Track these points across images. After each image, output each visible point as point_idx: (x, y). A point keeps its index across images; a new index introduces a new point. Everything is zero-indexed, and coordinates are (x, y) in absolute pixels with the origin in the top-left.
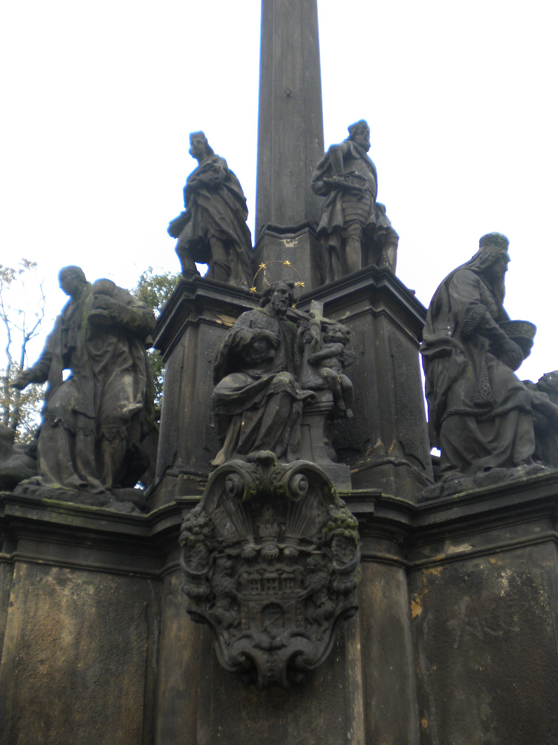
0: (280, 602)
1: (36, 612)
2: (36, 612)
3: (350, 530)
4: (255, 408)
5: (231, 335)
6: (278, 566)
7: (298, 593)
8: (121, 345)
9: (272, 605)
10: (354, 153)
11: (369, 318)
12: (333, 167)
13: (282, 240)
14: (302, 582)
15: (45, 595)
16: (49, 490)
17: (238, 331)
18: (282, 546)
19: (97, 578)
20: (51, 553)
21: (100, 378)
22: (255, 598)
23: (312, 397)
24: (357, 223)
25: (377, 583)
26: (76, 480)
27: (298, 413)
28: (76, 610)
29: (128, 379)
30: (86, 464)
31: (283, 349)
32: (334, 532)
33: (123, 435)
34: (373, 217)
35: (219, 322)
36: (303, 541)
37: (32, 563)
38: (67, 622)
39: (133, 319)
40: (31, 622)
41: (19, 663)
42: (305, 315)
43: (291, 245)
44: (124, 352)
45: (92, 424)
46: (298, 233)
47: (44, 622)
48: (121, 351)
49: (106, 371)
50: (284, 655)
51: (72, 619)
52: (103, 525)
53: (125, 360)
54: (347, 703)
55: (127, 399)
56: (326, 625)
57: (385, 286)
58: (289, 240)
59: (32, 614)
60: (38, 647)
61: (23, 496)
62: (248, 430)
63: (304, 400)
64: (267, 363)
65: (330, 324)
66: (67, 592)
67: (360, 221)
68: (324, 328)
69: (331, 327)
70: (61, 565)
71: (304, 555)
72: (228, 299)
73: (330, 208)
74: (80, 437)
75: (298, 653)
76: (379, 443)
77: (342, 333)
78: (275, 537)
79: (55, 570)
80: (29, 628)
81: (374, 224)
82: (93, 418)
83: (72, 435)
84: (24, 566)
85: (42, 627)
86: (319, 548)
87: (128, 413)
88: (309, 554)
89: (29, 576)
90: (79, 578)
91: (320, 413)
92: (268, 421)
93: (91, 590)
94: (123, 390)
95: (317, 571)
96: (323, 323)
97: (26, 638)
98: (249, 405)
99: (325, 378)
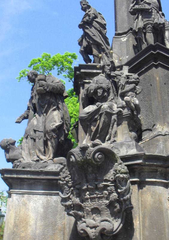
0: (98, 207)
1: (20, 212)
2: (20, 212)
3: (123, 174)
5: (86, 90)
7: (105, 202)
8: (51, 100)
13: (121, 39)
15: (23, 205)
16: (24, 164)
17: (89, 87)
18: (96, 183)
23: (120, 111)
24: (149, 24)
25: (148, 193)
27: (115, 119)
31: (111, 91)
32: (116, 176)
33: (54, 137)
38: (32, 215)
40: (18, 216)
41: (14, 233)
44: (53, 102)
45: (42, 134)
46: (127, 34)
47: (23, 216)
48: (52, 102)
50: (98, 229)
51: (33, 214)
55: (55, 121)
57: (152, 52)
58: (123, 38)
59: (18, 213)
60: (21, 226)
61: (13, 169)
63: (117, 113)
64: (104, 99)
65: (131, 75)
67: (150, 23)
68: (128, 77)
69: (130, 77)
73: (137, 20)
77: (135, 79)
78: (93, 180)
80: (17, 219)
81: (157, 23)
82: (42, 132)
85: (22, 218)
87: (25, 187)
88: (108, 186)
92: (101, 126)
93: (41, 202)
95: (112, 193)
97: (16, 223)
99: (126, 102)
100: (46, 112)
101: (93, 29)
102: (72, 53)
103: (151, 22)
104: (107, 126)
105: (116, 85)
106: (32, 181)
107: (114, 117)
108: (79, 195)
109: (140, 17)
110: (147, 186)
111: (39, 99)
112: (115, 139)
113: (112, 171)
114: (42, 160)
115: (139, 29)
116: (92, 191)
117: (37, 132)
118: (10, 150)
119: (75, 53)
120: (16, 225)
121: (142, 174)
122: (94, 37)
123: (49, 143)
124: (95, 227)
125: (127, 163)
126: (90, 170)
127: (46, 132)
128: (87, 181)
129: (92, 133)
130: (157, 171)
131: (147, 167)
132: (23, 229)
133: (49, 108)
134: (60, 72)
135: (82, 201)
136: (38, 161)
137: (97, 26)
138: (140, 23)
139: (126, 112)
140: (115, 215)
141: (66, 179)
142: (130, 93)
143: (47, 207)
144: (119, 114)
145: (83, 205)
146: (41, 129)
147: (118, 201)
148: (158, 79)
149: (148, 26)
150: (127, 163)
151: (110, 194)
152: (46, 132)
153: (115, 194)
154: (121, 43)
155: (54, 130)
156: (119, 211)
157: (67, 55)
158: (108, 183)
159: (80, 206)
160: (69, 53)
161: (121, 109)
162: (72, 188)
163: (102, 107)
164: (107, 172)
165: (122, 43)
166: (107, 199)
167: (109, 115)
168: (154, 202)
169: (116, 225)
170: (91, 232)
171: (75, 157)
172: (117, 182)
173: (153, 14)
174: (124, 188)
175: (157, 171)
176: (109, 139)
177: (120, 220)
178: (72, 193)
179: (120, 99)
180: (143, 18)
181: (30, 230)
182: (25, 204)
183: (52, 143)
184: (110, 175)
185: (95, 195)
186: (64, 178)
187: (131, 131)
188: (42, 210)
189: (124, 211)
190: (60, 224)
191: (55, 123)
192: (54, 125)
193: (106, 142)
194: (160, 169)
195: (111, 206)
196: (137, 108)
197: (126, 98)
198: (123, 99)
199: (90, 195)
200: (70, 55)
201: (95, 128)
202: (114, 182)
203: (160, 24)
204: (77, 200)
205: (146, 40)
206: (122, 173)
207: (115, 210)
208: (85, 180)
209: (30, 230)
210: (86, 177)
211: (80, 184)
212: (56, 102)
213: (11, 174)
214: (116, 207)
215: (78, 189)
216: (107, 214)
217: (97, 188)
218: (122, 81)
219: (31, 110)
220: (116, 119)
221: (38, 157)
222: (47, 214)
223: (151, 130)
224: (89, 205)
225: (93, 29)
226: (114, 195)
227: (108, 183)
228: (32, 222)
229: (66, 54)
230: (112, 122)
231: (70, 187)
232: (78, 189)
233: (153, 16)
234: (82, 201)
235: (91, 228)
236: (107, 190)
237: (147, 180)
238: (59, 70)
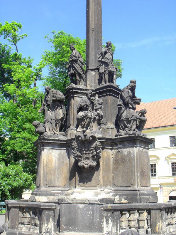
9: (88, 157)
10: (108, 52)
12: (93, 135)
23: (95, 117)
29: (61, 110)
30: (54, 129)
31: (90, 106)
42: (94, 98)
43: (93, 74)
50: (89, 165)
55: (61, 115)
64: (86, 109)
68: (98, 100)
69: (99, 101)
72: (80, 91)
74: (53, 124)
75: (91, 165)
81: (111, 71)
87: (50, 146)
88: (93, 149)
93: (57, 153)
94: (60, 113)
96: (98, 100)
99: (98, 113)
100: (56, 110)
101: (77, 65)
102: (18, 24)
103: (108, 69)
104: (89, 123)
105: (93, 104)
106: (54, 143)
107: (92, 119)
108: (80, 152)
109: (103, 65)
110: (105, 149)
111: (52, 102)
112: (92, 129)
113: (94, 144)
114: (56, 133)
115: (102, 72)
116: (86, 151)
117: (52, 120)
118: (38, 127)
119: (21, 24)
120: (47, 163)
121: (103, 145)
122: (78, 70)
123: (58, 125)
124: (87, 164)
125: (100, 140)
126: (86, 143)
127: (56, 120)
128: (85, 147)
129: (82, 125)
130: (109, 144)
131: (106, 142)
132: (50, 164)
133: (57, 108)
134: (6, 37)
135: (82, 154)
136: (54, 134)
137: (80, 64)
138: (103, 69)
139: (97, 118)
140: (94, 160)
141: (76, 145)
142: (99, 109)
143: (60, 155)
144: (95, 118)
145: (82, 156)
146: (54, 118)
147: (96, 155)
148: (110, 101)
149: (107, 71)
150: (100, 140)
151: (93, 152)
152: (56, 120)
153: (95, 152)
154: (91, 76)
155: (60, 120)
156: (96, 159)
157: (14, 24)
158: (93, 148)
159: (81, 156)
160: (16, 23)
161: (95, 116)
162: (78, 149)
163: (88, 115)
164: (93, 144)
165: (92, 76)
166: (92, 154)
167: (91, 118)
168: (107, 156)
169: (94, 164)
170: (86, 166)
171: (81, 138)
172: (96, 148)
173: (110, 65)
174: (99, 151)
175: (109, 144)
176: (90, 128)
177: (96, 162)
178: (78, 151)
179: (95, 112)
180: (105, 66)
181: (53, 165)
182: (51, 154)
183: (59, 125)
184: (94, 145)
185: (87, 153)
186: (75, 145)
187: (98, 125)
188: (58, 156)
189: (97, 158)
190: (65, 162)
193: (88, 129)
194: (110, 143)
195: (93, 157)
196: (102, 116)
197: (98, 111)
198: (96, 111)
199: (85, 152)
200: (16, 25)
201: (84, 123)
202: (95, 148)
203: (112, 71)
204: (80, 154)
205: (105, 78)
207: (95, 158)
208: (83, 146)
209: (53, 165)
211: (81, 148)
212: (61, 105)
213: (45, 140)
214: (95, 157)
215: (80, 150)
216: (91, 160)
217: (88, 150)
218: (96, 103)
219: (46, 106)
220: (93, 120)
221: (54, 132)
222: (60, 158)
223: (105, 124)
224: (84, 156)
225: (77, 65)
226: (95, 153)
227: (93, 148)
228: (54, 161)
229: (12, 23)
230: (91, 121)
231: (77, 149)
232: (80, 150)
233: (109, 66)
234: (82, 154)
235: (86, 164)
236: (92, 151)
237: (105, 147)
238: (6, 35)
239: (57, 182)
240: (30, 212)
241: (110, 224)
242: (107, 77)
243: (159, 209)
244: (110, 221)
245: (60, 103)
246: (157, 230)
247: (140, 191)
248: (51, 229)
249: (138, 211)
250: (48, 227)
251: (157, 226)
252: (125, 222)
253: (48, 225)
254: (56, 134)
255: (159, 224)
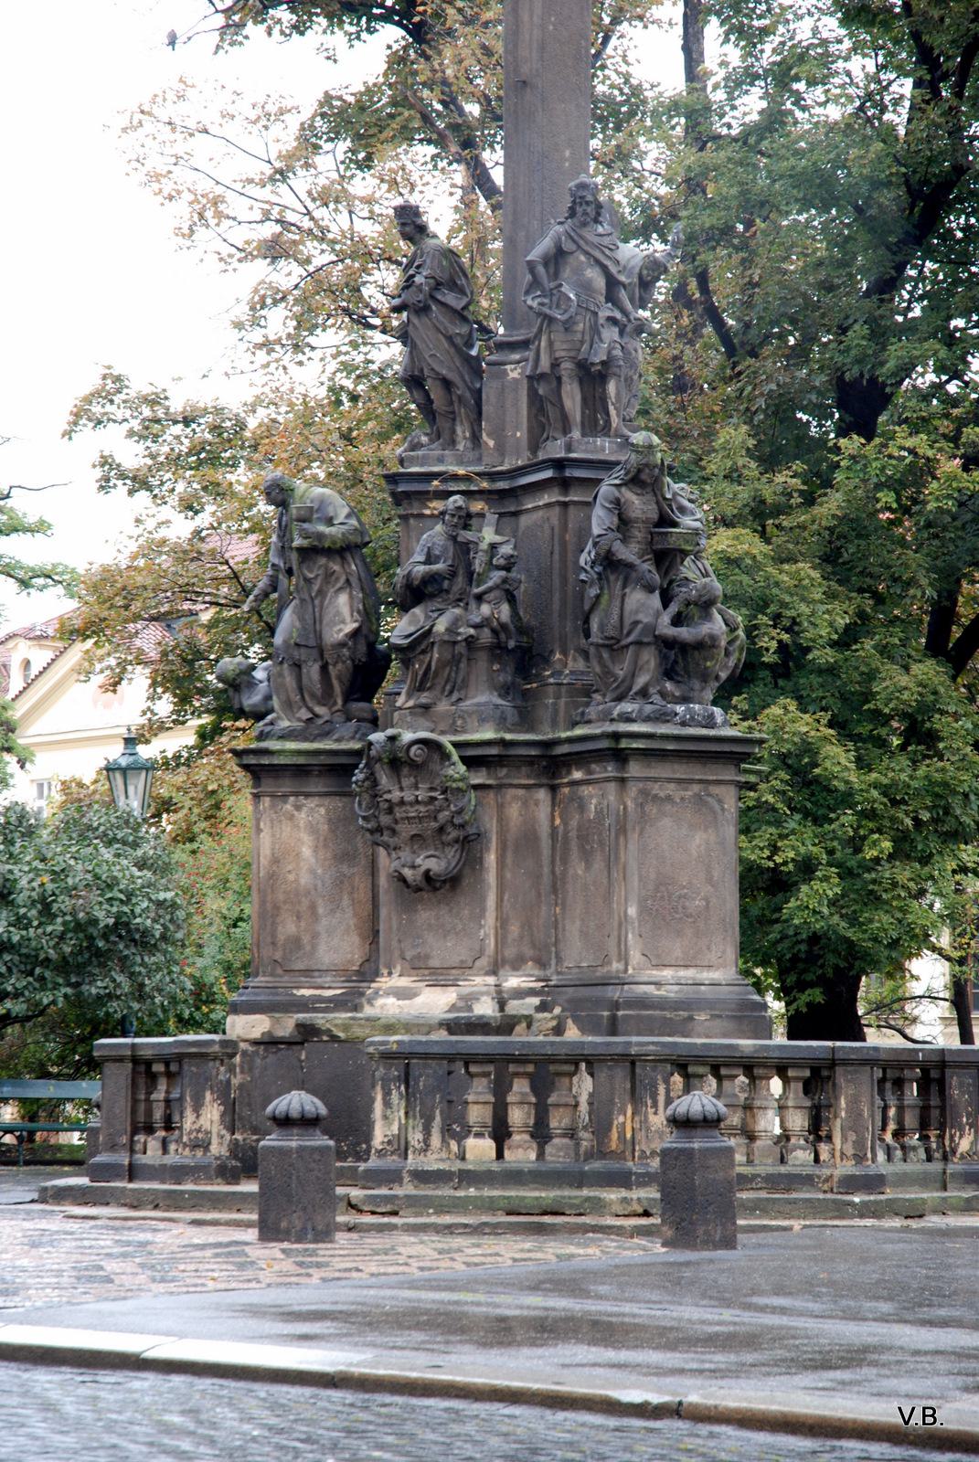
4: (424, 652)
6: (417, 807)
8: (331, 564)
11: (557, 509)
14: (435, 817)
19: (327, 801)
20: (286, 786)
21: (317, 602)
22: (406, 830)
26: (304, 714)
28: (313, 829)
31: (461, 572)
34: (585, 347)
35: (427, 512)
36: (432, 789)
37: (273, 796)
39: (334, 543)
49: (321, 593)
52: (323, 760)
53: (337, 579)
54: (483, 899)
55: (343, 622)
56: (456, 846)
62: (421, 673)
66: (303, 815)
70: (296, 794)
71: (433, 799)
76: (558, 656)
79: (292, 799)
83: (297, 666)
84: (267, 799)
86: (443, 793)
88: (436, 799)
89: (273, 806)
90: (311, 803)
91: (483, 648)
93: (322, 811)
94: (338, 613)
98: (419, 650)
120: (275, 860)
163: (435, 629)
191: (342, 626)
192: (340, 630)
206: (455, 781)
210: (400, 782)
221: (311, 710)
239: (322, 948)
240: (330, 1110)
241: (395, 1108)
242: (572, 398)
243: (624, 1061)
244: (395, 1096)
245: (343, 559)
246: (614, 1145)
247: (626, 987)
248: (208, 1133)
249: (589, 1064)
250: (196, 1126)
251: (614, 1130)
252: (480, 1106)
253: (198, 1117)
254: (320, 721)
255: (621, 1119)
